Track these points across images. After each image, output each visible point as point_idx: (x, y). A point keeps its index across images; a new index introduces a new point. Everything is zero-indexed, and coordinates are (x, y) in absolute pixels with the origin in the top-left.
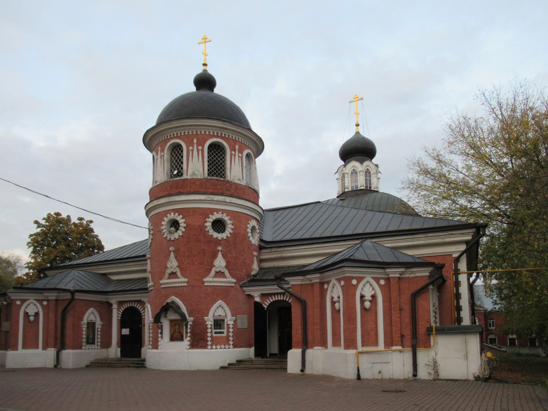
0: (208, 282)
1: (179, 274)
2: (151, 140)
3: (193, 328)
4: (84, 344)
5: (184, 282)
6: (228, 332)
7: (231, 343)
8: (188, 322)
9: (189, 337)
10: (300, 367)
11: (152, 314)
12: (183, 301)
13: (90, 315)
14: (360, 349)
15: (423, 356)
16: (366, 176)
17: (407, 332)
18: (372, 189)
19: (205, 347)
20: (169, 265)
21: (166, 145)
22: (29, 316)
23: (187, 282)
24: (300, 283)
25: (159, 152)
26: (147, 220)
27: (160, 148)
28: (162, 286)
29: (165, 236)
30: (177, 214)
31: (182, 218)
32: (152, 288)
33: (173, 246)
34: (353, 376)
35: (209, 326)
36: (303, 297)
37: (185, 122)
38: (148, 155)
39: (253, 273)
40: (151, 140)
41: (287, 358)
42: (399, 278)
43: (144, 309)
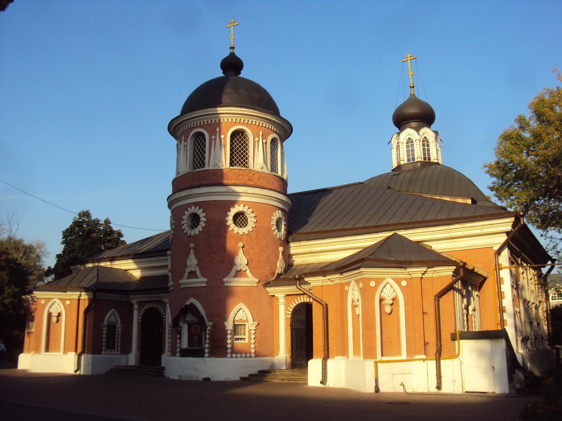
1: (198, 273)
2: (175, 128)
3: (211, 334)
4: (104, 348)
6: (250, 338)
8: (207, 327)
9: (208, 343)
10: (435, 384)
12: (202, 303)
13: (110, 316)
14: (379, 358)
16: (424, 145)
17: (431, 338)
19: (224, 355)
20: (188, 263)
21: (189, 136)
23: (207, 283)
24: (320, 284)
27: (183, 138)
29: (185, 232)
30: (197, 208)
31: (203, 212)
32: (172, 288)
33: (193, 242)
35: (229, 332)
36: (326, 300)
37: (208, 111)
38: (174, 142)
40: (175, 128)
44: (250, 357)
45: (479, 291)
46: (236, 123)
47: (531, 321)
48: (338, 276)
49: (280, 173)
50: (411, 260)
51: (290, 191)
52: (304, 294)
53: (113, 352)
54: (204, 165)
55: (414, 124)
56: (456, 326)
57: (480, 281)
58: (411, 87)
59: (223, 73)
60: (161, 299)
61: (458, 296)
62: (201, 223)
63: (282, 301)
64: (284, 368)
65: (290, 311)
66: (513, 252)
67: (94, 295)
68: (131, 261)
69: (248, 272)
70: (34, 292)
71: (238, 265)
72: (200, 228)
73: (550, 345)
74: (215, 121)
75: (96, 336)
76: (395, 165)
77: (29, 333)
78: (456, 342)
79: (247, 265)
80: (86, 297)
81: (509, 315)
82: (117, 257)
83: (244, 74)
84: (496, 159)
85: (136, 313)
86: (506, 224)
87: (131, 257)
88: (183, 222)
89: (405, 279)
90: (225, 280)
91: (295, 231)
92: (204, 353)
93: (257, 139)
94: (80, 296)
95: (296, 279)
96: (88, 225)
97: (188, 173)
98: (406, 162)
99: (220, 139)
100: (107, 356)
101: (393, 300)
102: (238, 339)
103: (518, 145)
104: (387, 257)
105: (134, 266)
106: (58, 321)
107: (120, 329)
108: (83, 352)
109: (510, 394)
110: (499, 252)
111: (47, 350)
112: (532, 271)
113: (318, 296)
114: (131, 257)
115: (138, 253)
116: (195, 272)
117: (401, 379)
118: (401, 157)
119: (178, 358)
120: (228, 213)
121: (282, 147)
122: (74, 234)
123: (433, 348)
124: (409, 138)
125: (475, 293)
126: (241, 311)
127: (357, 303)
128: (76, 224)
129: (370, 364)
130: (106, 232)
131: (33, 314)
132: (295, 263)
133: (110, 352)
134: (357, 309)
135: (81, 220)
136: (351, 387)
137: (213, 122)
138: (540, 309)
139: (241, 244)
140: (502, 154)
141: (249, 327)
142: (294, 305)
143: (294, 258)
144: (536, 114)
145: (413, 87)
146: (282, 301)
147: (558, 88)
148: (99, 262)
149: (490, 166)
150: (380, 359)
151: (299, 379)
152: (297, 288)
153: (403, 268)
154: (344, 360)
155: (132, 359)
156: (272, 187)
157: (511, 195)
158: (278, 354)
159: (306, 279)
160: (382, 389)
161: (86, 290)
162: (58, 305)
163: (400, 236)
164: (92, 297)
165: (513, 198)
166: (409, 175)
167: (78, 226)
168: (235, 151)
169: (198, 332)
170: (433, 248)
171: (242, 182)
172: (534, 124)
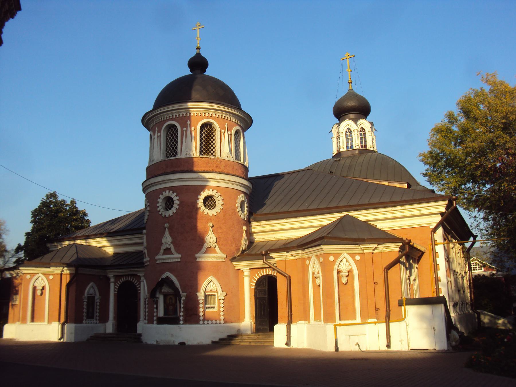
2: (148, 121)
4: (85, 318)
5: (177, 258)
6: (219, 307)
8: (181, 297)
9: (183, 312)
10: (385, 343)
11: (148, 289)
14: (338, 322)
16: (361, 135)
17: (382, 304)
18: (368, 148)
20: (164, 241)
23: (181, 258)
24: (284, 259)
25: (156, 132)
26: (143, 196)
28: (157, 262)
30: (171, 192)
31: (176, 196)
32: (148, 263)
33: (168, 222)
35: (201, 302)
36: (288, 272)
37: (179, 106)
38: (147, 133)
40: (148, 121)
43: (140, 284)
44: (220, 323)
45: (418, 263)
46: (205, 117)
47: (459, 289)
48: (300, 251)
49: (242, 161)
50: (364, 238)
51: (250, 175)
52: (270, 267)
53: (92, 321)
54: (176, 153)
55: (352, 116)
56: (402, 294)
57: (419, 255)
58: (349, 83)
59: (191, 71)
60: (135, 273)
61: (403, 268)
62: (174, 205)
63: (246, 273)
64: (249, 332)
65: (253, 282)
66: (446, 231)
67: (77, 270)
68: (104, 239)
69: (217, 249)
70: (20, 268)
71: (208, 242)
72: (174, 210)
73: (472, 309)
74: (186, 114)
75: (77, 307)
76: (335, 152)
77: (13, 305)
78: (403, 307)
79: (216, 242)
80: (68, 272)
81: (443, 285)
82: (91, 235)
83: (209, 72)
84: (430, 150)
85: (112, 286)
86: (441, 207)
87: (105, 235)
88: (158, 205)
89: (358, 254)
90: (197, 255)
91: (255, 212)
92: (179, 320)
93: (223, 131)
94: (63, 271)
95: (263, 255)
96: (55, 206)
97: (162, 161)
98: (345, 149)
99: (191, 131)
100: (87, 325)
101: (349, 272)
102: (209, 308)
103: (448, 137)
104: (342, 235)
105: (107, 244)
106: (42, 294)
107: (98, 301)
108: (66, 322)
109: (448, 350)
110: (434, 230)
111: (33, 320)
112: (459, 246)
113: (281, 268)
114: (105, 235)
115: (106, 230)
116: (170, 249)
117: (356, 339)
118: (341, 145)
119: (155, 325)
120: (199, 197)
121: (244, 138)
122: (42, 214)
123: (383, 313)
124: (348, 128)
125: (415, 266)
126: (212, 283)
127: (318, 275)
128: (44, 204)
129: (330, 327)
130: (72, 212)
131: (17, 289)
132: (256, 240)
134: (317, 280)
135: (48, 201)
136: (313, 348)
137: (185, 115)
138: (465, 278)
139: (210, 224)
140: (433, 145)
141: (218, 297)
143: (255, 236)
144: (463, 111)
145: (351, 83)
146: (246, 273)
147: (481, 89)
148: (74, 240)
149: (424, 156)
150: (338, 323)
151: (265, 342)
152: (264, 262)
153: (357, 244)
154: (306, 325)
155: (110, 327)
156: (237, 174)
157: (442, 180)
158: (243, 320)
159: (271, 255)
160: (341, 349)
161: (68, 266)
162: (42, 279)
163: (351, 217)
164: (74, 272)
165: (442, 183)
166: (348, 161)
167: (46, 206)
168: (204, 141)
169: (173, 302)
170: (377, 227)
171: (211, 169)
172: (462, 120)
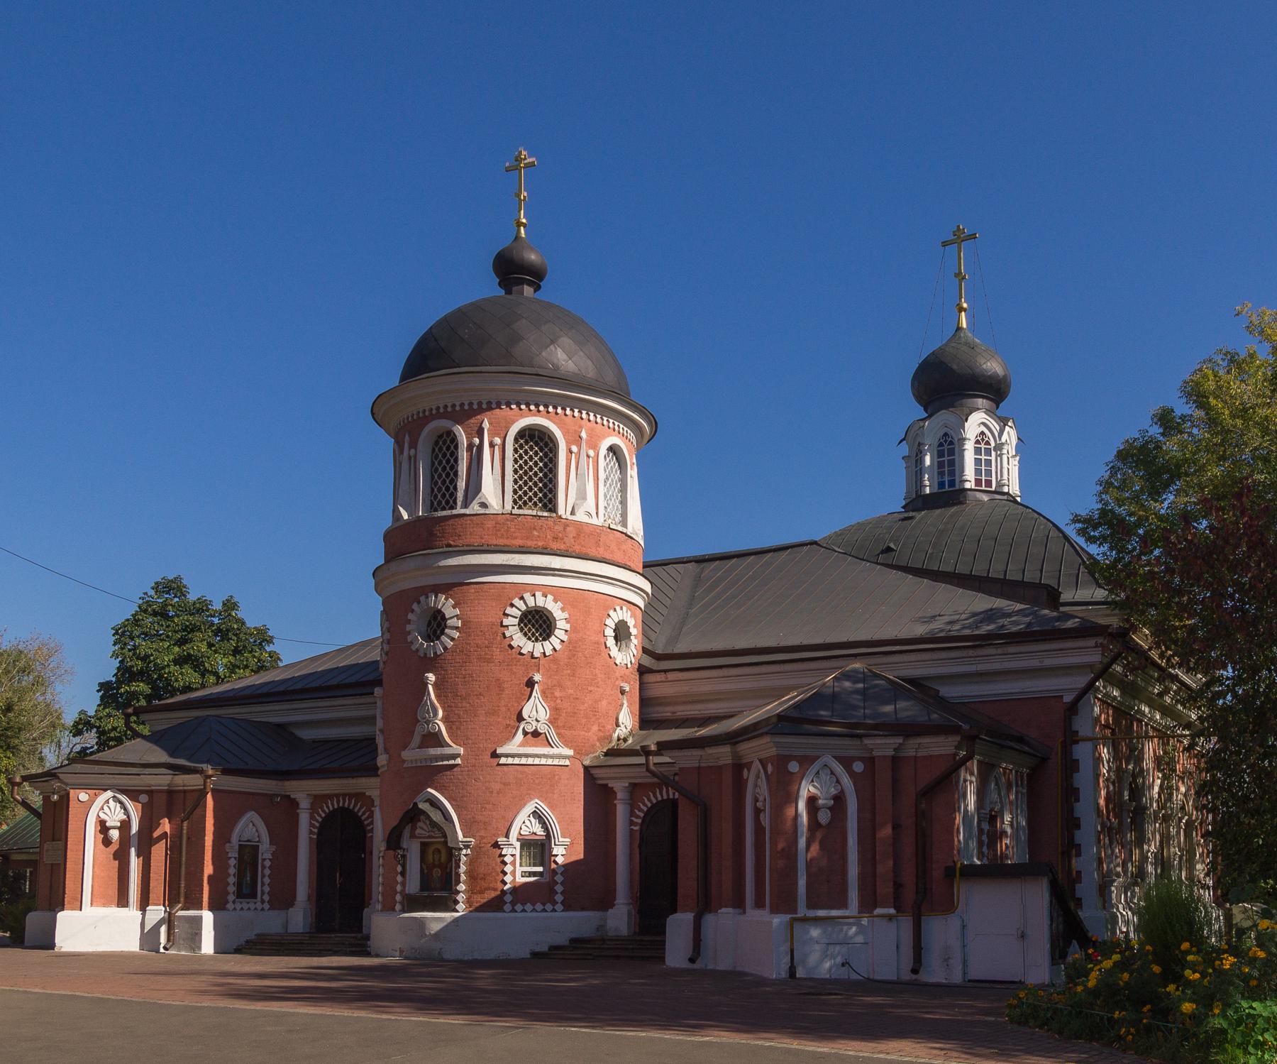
0: (507, 756)
4: (231, 898)
7: (559, 898)
14: (802, 911)
15: (941, 930)
22: (108, 829)
25: (406, 445)
34: (784, 974)
39: (621, 732)
41: (664, 933)
42: (893, 757)
53: (252, 906)
65: (638, 817)
124: (946, 434)
133: (245, 906)
142: (645, 804)
169: (443, 859)
171: (540, 544)
